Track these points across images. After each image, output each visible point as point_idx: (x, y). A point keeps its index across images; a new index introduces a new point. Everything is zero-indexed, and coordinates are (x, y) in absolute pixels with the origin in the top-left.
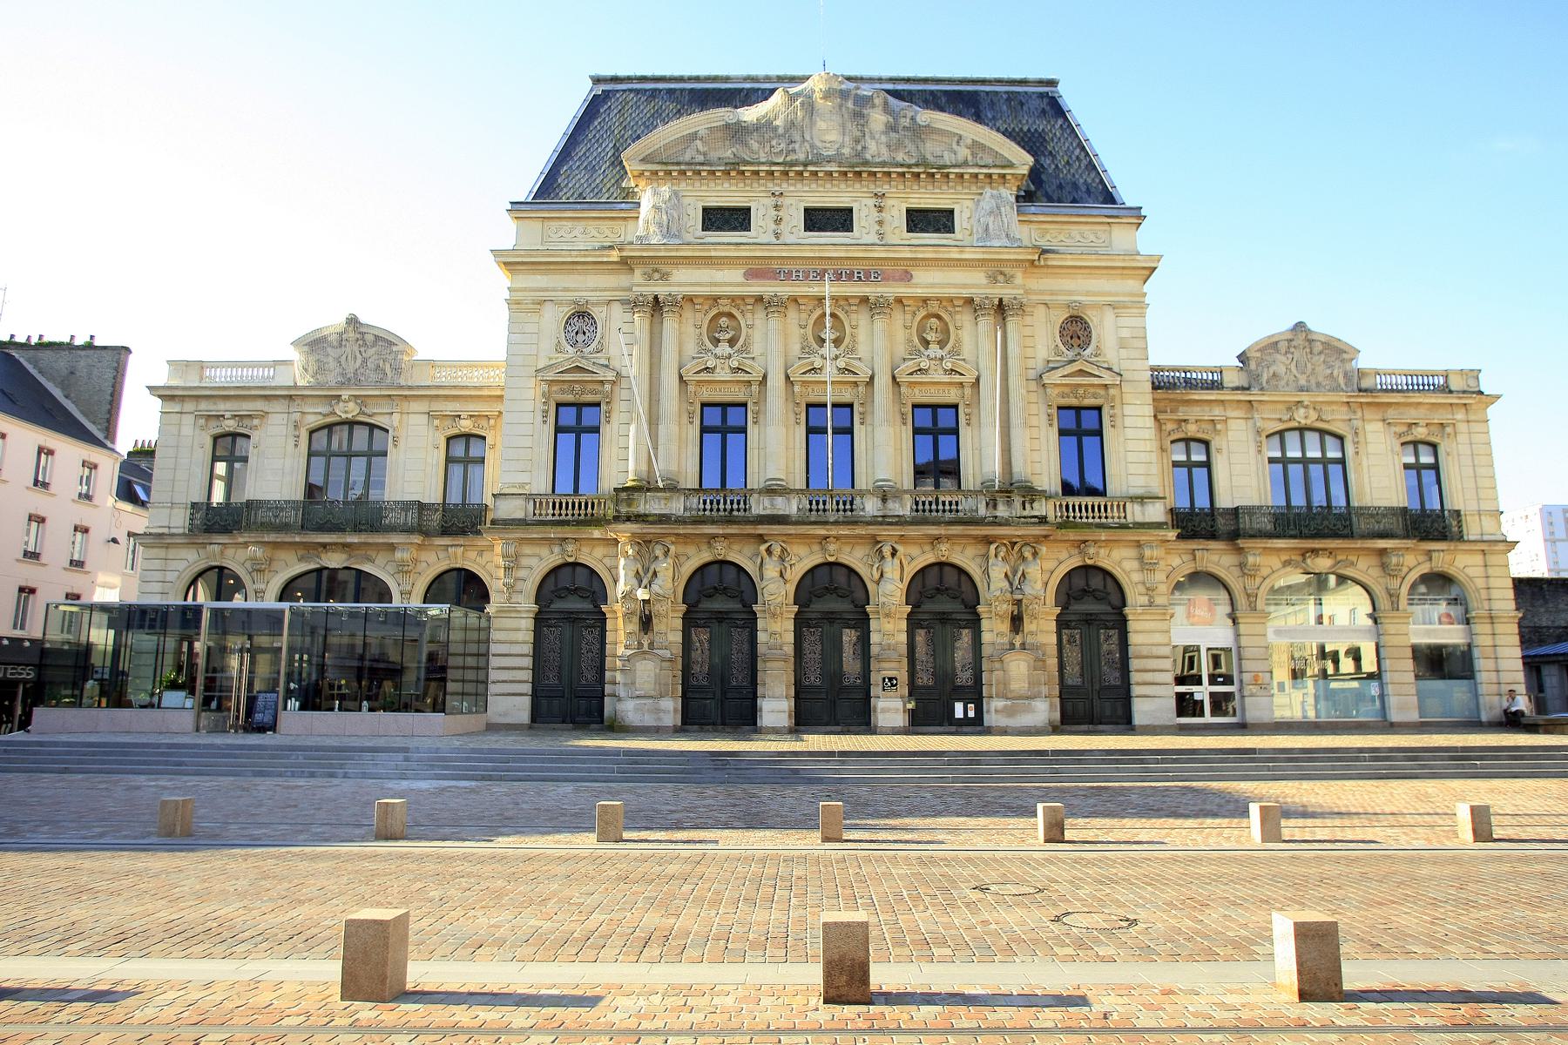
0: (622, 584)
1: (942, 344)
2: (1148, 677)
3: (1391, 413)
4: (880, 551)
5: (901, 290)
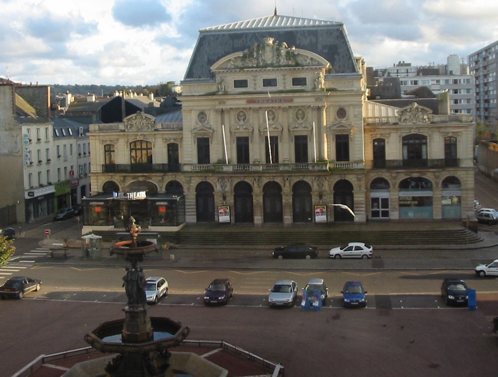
0: (218, 188)
3: (442, 130)
5: (290, 104)
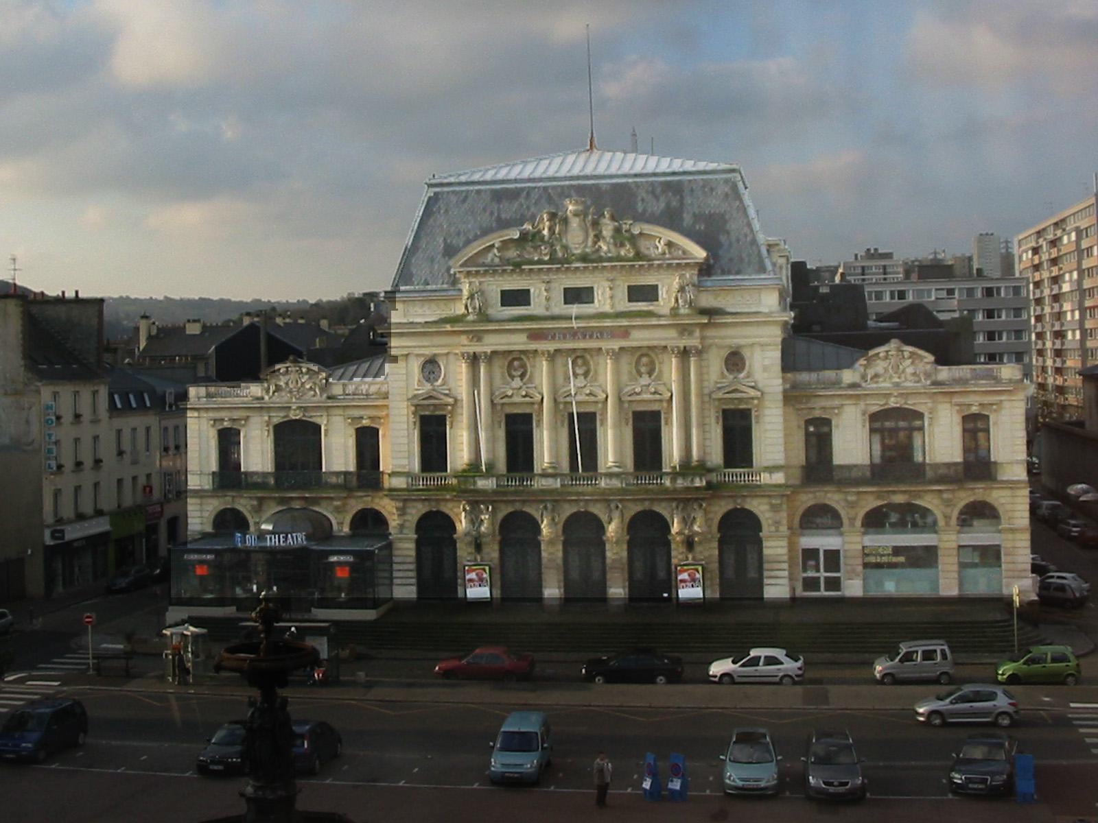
0: (462, 524)
1: (650, 374)
2: (773, 573)
5: (624, 343)
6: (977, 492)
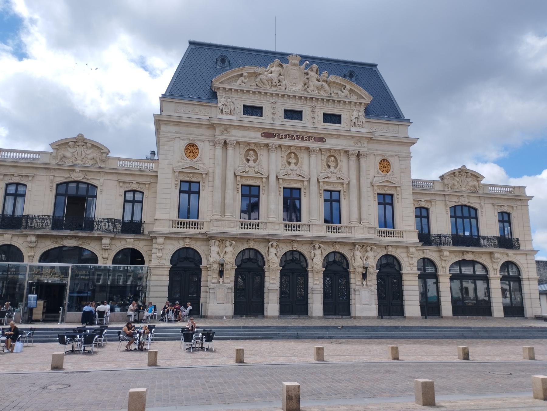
4: (314, 246)
6: (130, 242)
